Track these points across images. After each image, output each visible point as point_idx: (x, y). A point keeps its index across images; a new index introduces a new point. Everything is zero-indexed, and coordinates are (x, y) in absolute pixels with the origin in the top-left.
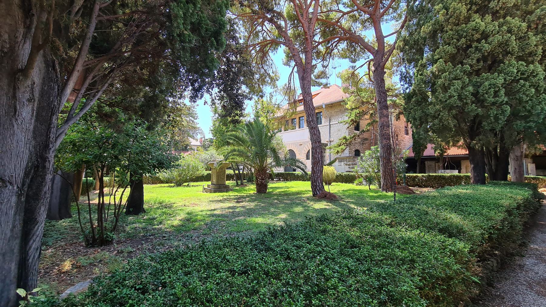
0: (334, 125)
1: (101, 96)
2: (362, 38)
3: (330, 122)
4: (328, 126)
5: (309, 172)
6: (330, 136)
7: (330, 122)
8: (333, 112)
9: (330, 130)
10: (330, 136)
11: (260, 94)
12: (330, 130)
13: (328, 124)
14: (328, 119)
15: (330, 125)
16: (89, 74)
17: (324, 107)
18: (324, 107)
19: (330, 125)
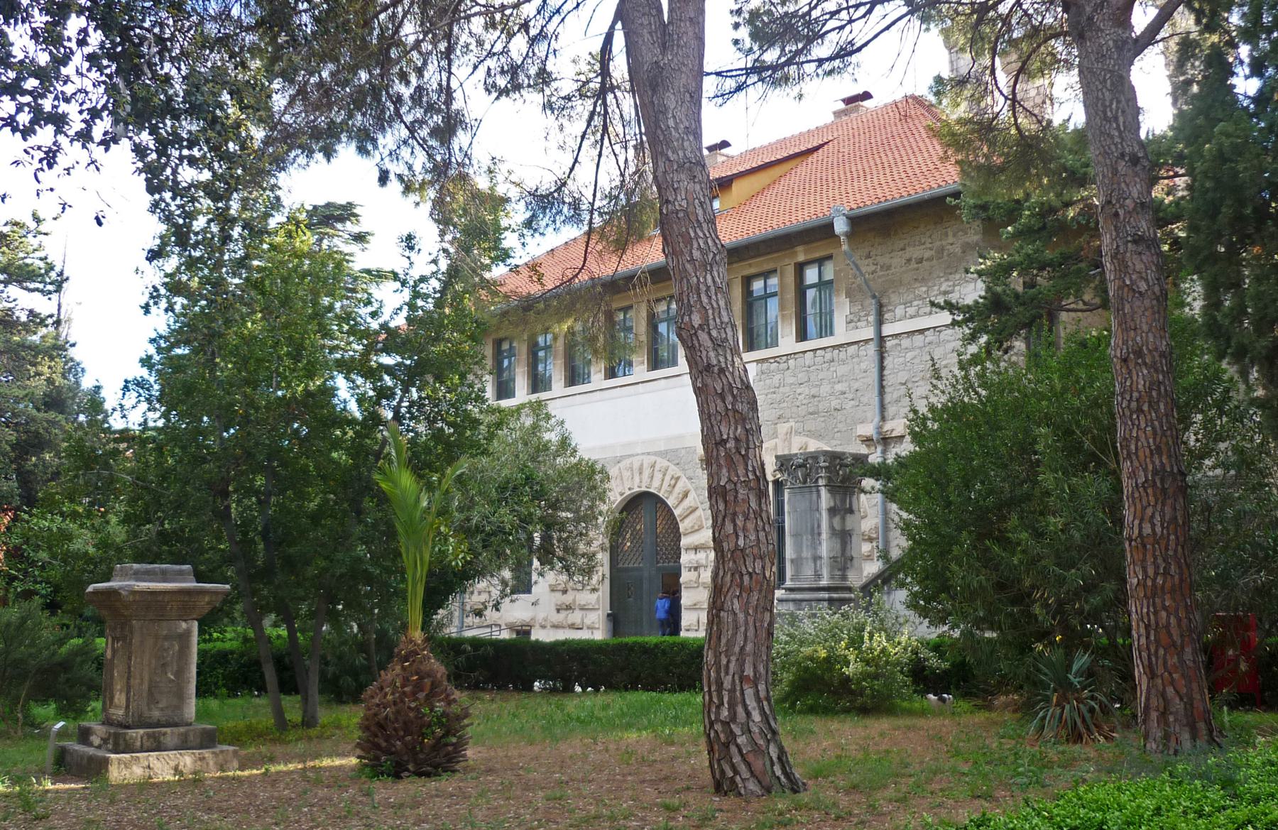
0: (906, 342)
1: (1105, 695)
2: (456, 639)
3: (880, 322)
4: (872, 349)
5: (732, 726)
6: (883, 407)
7: (880, 322)
8: (897, 260)
9: (882, 368)
10: (883, 407)
11: (155, 294)
12: (882, 368)
13: (869, 333)
14: (871, 305)
15: (881, 340)
16: (82, 757)
17: (840, 226)
18: (840, 226)
19: (881, 340)
